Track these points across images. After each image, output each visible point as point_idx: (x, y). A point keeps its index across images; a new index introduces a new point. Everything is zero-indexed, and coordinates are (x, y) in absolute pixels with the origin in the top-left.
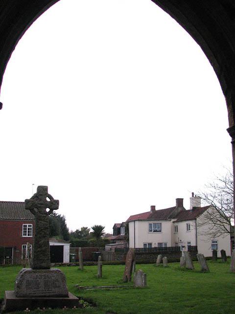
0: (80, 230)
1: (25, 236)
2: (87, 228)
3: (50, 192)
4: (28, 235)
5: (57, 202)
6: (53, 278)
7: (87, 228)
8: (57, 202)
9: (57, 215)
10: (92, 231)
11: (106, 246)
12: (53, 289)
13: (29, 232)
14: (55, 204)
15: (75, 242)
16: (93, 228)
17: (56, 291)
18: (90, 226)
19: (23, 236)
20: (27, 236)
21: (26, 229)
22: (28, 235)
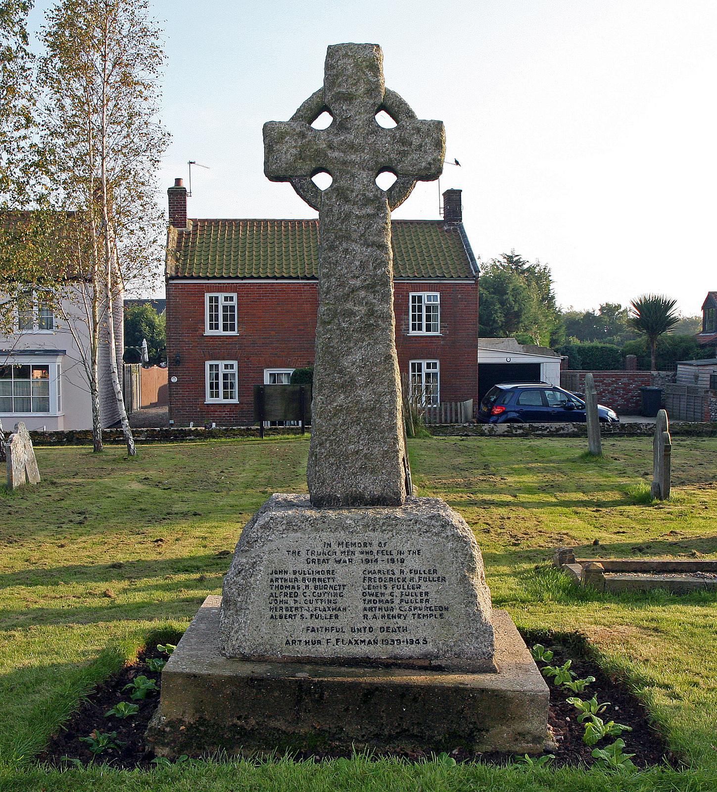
0: (597, 313)
1: (417, 333)
2: (620, 306)
3: (393, 79)
4: (225, 329)
5: (435, 132)
6: (413, 562)
7: (620, 306)
8: (435, 132)
9: (526, 266)
10: (633, 314)
11: (680, 368)
12: (410, 621)
13: (428, 318)
14: (419, 150)
15: (581, 350)
16: (637, 306)
17: (420, 636)
18: (626, 297)
19: (412, 333)
20: (424, 333)
21: (420, 309)
22: (428, 330)
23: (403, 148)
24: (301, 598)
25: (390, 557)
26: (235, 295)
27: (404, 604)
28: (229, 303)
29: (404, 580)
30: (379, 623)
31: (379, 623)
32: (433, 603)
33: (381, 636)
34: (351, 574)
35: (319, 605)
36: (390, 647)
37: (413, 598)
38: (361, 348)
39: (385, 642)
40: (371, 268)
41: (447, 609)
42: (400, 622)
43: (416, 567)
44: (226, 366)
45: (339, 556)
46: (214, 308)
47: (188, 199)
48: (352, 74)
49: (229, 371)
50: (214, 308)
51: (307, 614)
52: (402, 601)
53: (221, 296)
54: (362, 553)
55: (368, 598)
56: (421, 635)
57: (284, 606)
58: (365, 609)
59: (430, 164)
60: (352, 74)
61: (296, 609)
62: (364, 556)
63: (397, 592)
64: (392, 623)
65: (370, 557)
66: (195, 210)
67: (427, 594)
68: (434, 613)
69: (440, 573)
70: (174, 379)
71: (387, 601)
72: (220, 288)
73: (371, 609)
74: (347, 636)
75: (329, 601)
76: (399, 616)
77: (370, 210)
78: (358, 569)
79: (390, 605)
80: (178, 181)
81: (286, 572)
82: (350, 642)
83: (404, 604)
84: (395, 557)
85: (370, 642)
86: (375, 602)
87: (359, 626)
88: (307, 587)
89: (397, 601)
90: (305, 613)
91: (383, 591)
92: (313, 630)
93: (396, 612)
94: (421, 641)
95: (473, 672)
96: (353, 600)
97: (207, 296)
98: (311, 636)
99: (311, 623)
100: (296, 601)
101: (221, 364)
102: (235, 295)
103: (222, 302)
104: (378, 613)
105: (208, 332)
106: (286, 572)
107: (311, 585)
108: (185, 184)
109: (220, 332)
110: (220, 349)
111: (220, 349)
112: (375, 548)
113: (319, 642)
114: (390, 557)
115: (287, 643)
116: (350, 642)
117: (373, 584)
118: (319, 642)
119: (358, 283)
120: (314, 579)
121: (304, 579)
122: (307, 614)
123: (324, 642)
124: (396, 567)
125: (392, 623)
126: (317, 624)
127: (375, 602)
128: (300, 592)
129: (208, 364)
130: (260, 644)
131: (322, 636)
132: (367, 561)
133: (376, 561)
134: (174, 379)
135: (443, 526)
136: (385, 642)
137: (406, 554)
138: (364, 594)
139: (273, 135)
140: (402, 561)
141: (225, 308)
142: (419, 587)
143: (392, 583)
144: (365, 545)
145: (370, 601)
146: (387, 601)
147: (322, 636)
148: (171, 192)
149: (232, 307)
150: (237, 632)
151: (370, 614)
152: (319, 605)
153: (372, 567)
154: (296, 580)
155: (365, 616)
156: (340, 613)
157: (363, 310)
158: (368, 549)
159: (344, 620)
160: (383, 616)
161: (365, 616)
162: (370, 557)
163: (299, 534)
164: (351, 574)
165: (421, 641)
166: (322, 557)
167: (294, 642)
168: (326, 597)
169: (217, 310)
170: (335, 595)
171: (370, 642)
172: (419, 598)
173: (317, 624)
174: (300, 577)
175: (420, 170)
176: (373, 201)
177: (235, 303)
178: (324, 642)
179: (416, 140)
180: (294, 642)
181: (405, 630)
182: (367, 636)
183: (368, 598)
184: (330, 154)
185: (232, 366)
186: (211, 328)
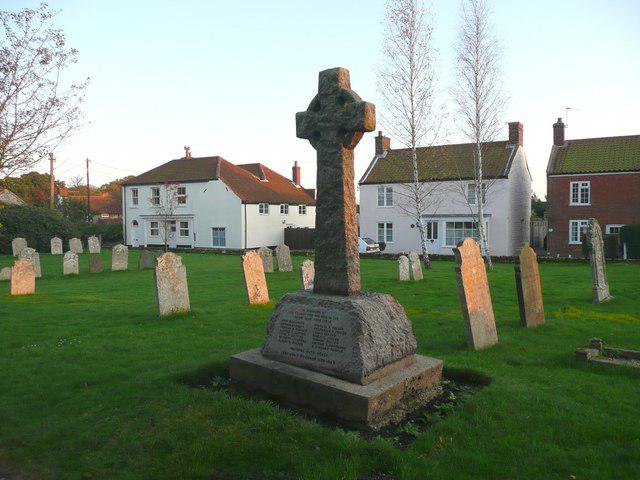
6: (334, 324)
26: (589, 183)
30: (316, 351)
31: (316, 351)
44: (582, 223)
46: (575, 190)
47: (195, 154)
48: (332, 85)
50: (575, 190)
53: (580, 183)
60: (332, 85)
70: (551, 230)
72: (580, 179)
77: (334, 150)
78: (313, 323)
80: (559, 120)
95: (295, 366)
97: (571, 183)
98: (291, 351)
99: (292, 346)
101: (579, 222)
102: (589, 183)
103: (580, 187)
105: (572, 204)
108: (563, 121)
109: (579, 204)
119: (329, 186)
129: (571, 222)
134: (551, 230)
139: (300, 117)
148: (555, 126)
149: (587, 190)
177: (588, 187)
179: (353, 112)
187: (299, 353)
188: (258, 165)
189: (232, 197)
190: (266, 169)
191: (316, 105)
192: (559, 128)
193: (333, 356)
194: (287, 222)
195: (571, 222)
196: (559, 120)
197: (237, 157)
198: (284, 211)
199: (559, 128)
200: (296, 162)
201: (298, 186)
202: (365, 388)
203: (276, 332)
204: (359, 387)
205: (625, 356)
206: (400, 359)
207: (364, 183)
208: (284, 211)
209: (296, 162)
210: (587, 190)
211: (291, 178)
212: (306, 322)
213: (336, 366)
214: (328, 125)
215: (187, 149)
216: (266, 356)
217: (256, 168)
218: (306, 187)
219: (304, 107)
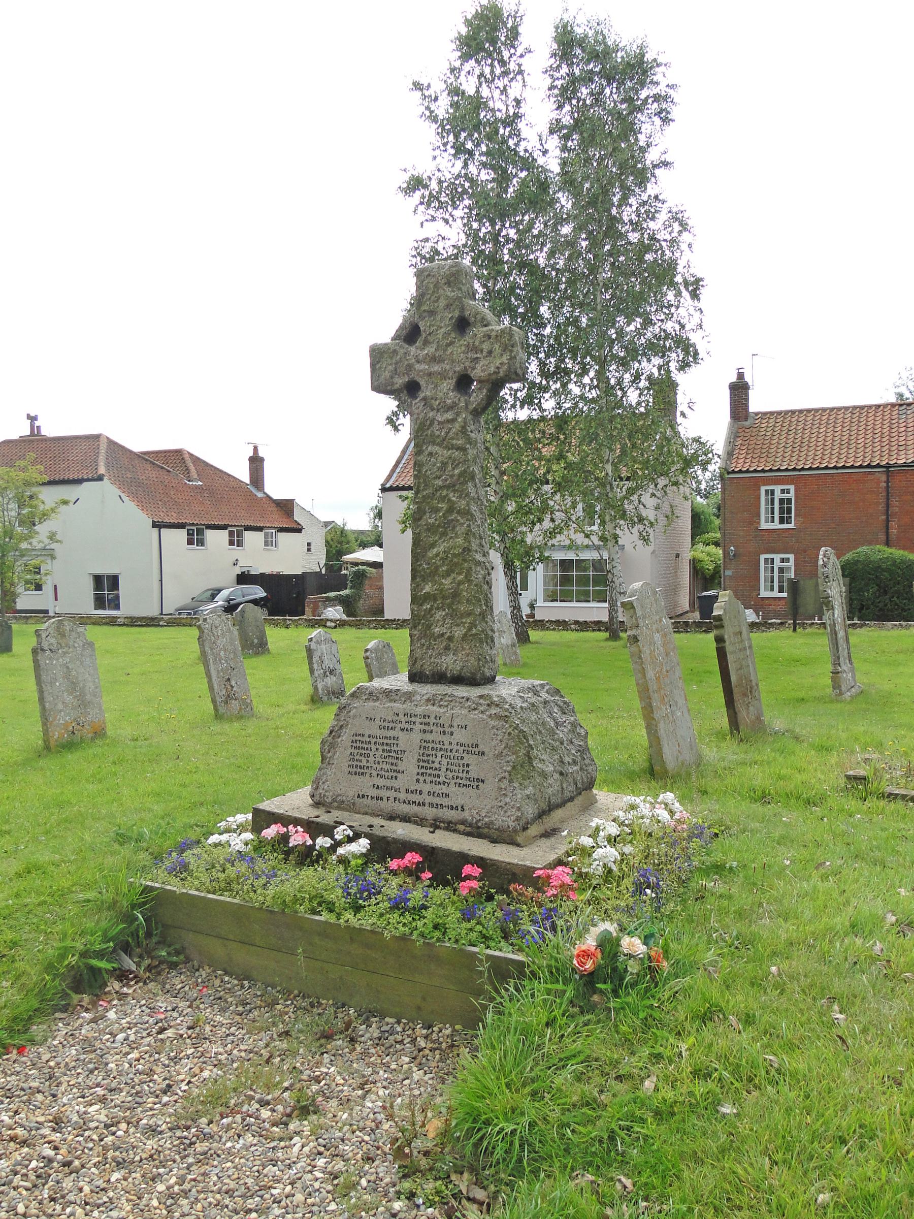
4: (782, 521)
6: (460, 736)
23: (475, 356)
24: (371, 759)
25: (442, 729)
26: (792, 488)
27: (448, 772)
28: (785, 496)
29: (451, 751)
30: (426, 788)
31: (426, 788)
32: (473, 774)
33: (429, 799)
34: (410, 742)
35: (384, 766)
36: (434, 810)
37: (457, 768)
38: (444, 541)
39: (431, 805)
40: (450, 468)
41: (483, 781)
42: (444, 789)
43: (462, 741)
45: (404, 725)
49: (785, 564)
51: (375, 773)
52: (447, 769)
53: (777, 489)
54: (421, 724)
55: (421, 764)
56: (459, 802)
57: (359, 764)
58: (418, 774)
59: (498, 368)
61: (368, 767)
62: (423, 727)
63: (444, 761)
64: (438, 789)
65: (426, 728)
66: (757, 403)
67: (468, 765)
68: (472, 784)
69: (481, 748)
71: (436, 769)
72: (777, 481)
73: (422, 774)
74: (402, 796)
75: (392, 764)
76: (444, 783)
79: (437, 772)
80: (741, 376)
81: (363, 735)
82: (404, 802)
83: (448, 772)
84: (447, 730)
85: (419, 804)
86: (426, 768)
87: (412, 788)
88: (377, 749)
89: (443, 769)
90: (373, 771)
91: (434, 759)
92: (378, 787)
93: (442, 779)
94: (459, 808)
96: (410, 765)
98: (375, 792)
100: (368, 761)
101: (777, 557)
103: (778, 495)
104: (428, 779)
105: (764, 525)
106: (363, 735)
107: (381, 748)
108: (748, 378)
109: (777, 525)
110: (774, 542)
111: (774, 542)
112: (432, 720)
113: (382, 799)
114: (442, 729)
115: (359, 796)
116: (404, 802)
117: (426, 752)
118: (382, 799)
120: (383, 744)
121: (375, 743)
122: (375, 773)
123: (385, 799)
124: (446, 739)
125: (438, 789)
126: (381, 782)
127: (426, 768)
128: (372, 754)
129: (763, 557)
130: (338, 795)
131: (384, 793)
132: (425, 732)
133: (431, 732)
135: (488, 705)
136: (431, 805)
137: (456, 727)
138: (419, 760)
139: (378, 354)
140: (452, 734)
141: (781, 501)
142: (462, 758)
143: (442, 753)
144: (424, 716)
145: (422, 767)
146: (436, 769)
147: (384, 793)
149: (789, 500)
150: (323, 783)
151: (422, 779)
152: (384, 766)
153: (429, 737)
154: (370, 742)
155: (418, 781)
156: (399, 775)
157: (444, 506)
158: (427, 720)
159: (402, 782)
160: (431, 782)
161: (418, 781)
162: (426, 728)
163: (377, 704)
164: (410, 742)
165: (459, 808)
166: (391, 725)
167: (363, 796)
168: (391, 760)
169: (773, 503)
170: (397, 758)
171: (419, 804)
172: (461, 768)
173: (381, 782)
174: (373, 741)
175: (490, 375)
176: (452, 407)
177: (792, 495)
178: (385, 799)
179: (486, 347)
180: (363, 796)
181: (447, 796)
182: (416, 798)
183: (421, 764)
184: (418, 367)
185: (788, 560)
186: (766, 522)
187: (391, 794)
188: (178, 452)
189: (134, 518)
190: (196, 460)
191: (410, 333)
192: (739, 390)
193: (458, 795)
194: (240, 564)
195: (763, 557)
196: (741, 376)
197: (142, 434)
198: (236, 541)
199: (739, 390)
200: (256, 448)
201: (260, 495)
202: (524, 852)
203: (341, 757)
204: (514, 850)
205: (435, 825)
206: (571, 799)
207: (391, 489)
208: (236, 541)
209: (256, 448)
210: (789, 500)
211: (246, 478)
212: (401, 735)
213: (466, 815)
214: (436, 368)
215: (32, 419)
216: (317, 804)
217: (175, 460)
218: (276, 496)
219: (386, 330)
